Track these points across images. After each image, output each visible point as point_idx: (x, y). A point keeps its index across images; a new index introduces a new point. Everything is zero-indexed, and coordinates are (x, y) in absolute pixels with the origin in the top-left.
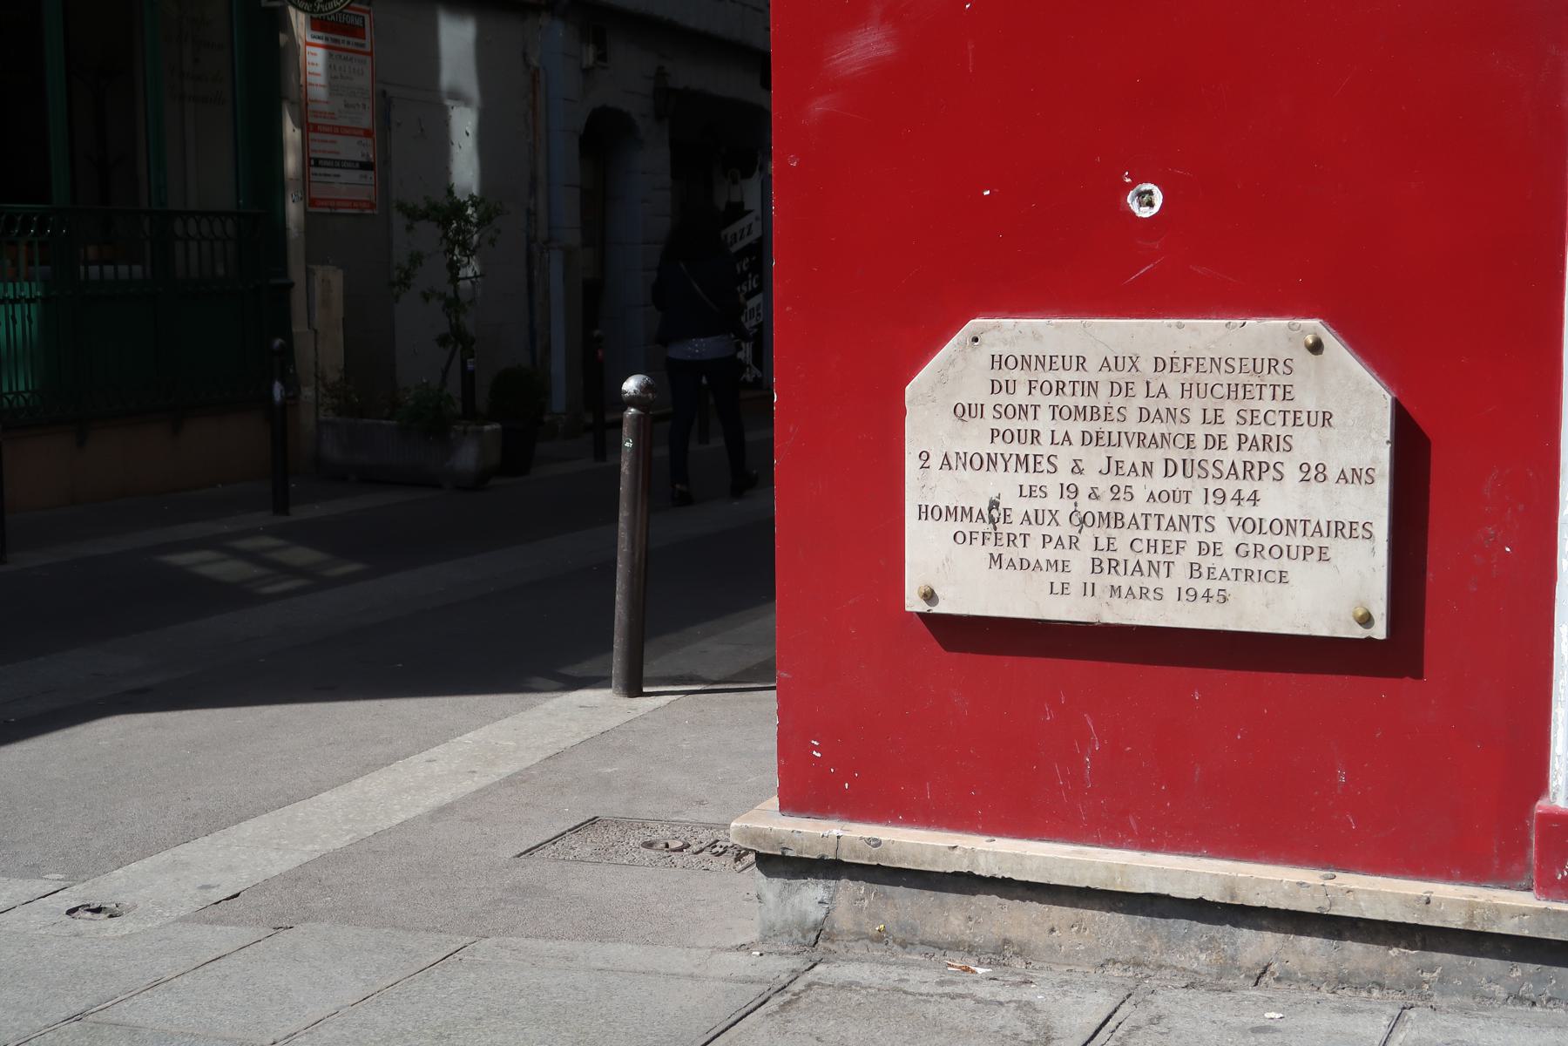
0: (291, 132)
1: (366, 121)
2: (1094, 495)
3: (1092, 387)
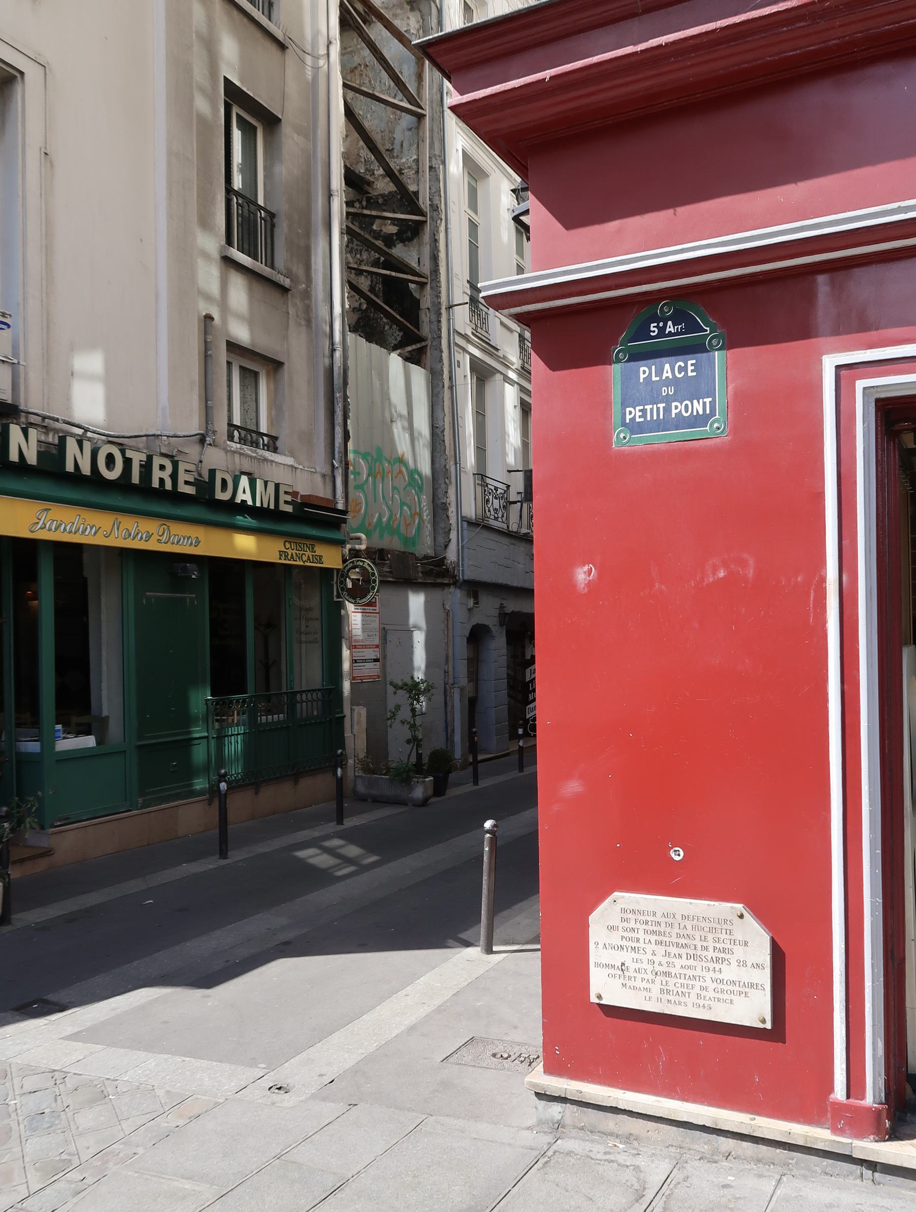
0: (346, 653)
1: (377, 641)
2: (660, 964)
3: (659, 923)
